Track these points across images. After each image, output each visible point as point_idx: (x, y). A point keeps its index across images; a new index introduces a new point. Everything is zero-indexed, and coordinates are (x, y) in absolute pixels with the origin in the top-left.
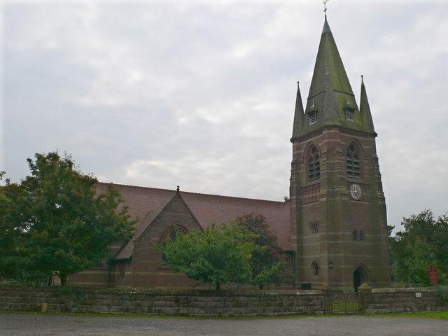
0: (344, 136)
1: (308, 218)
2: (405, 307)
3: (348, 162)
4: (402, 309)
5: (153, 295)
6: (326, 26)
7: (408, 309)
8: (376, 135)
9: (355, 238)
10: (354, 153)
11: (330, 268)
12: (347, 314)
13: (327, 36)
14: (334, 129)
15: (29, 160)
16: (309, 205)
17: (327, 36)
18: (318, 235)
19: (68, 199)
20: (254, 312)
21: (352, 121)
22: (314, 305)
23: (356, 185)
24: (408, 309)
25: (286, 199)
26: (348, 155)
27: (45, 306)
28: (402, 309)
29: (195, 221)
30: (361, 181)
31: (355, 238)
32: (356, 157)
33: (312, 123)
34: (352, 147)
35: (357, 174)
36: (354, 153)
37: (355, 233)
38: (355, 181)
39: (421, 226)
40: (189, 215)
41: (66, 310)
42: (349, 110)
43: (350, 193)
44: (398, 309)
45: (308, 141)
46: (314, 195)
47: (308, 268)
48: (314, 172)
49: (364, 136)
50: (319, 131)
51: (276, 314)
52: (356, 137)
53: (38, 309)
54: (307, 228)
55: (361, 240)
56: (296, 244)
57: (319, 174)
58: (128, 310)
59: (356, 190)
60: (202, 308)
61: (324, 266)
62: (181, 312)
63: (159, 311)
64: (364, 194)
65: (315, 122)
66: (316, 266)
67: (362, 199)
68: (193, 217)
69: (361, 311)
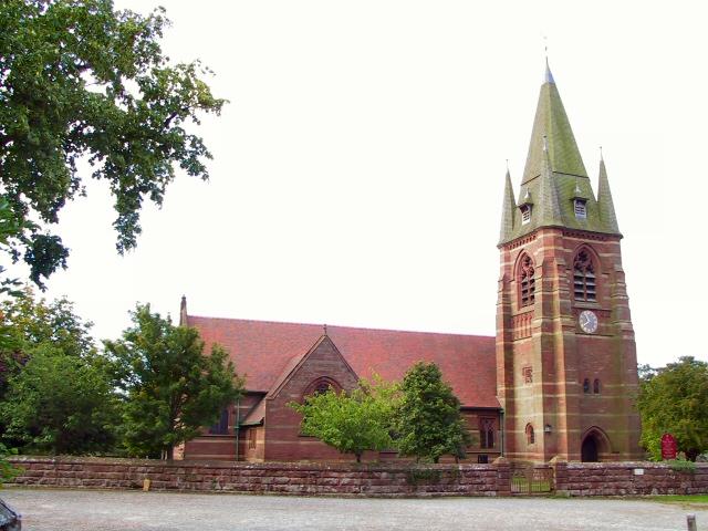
0: (570, 241)
1: (520, 362)
2: (618, 488)
3: (576, 278)
4: (612, 491)
5: (276, 470)
6: (550, 75)
7: (623, 492)
8: (620, 237)
9: (586, 390)
10: (587, 263)
11: (546, 433)
12: (531, 495)
13: (551, 94)
14: (572, 246)
15: (64, 267)
16: (522, 342)
17: (551, 94)
18: (531, 386)
19: (428, 414)
20: (400, 491)
21: (582, 220)
22: (482, 483)
23: (589, 312)
24: (623, 492)
25: (93, 74)
26: (577, 268)
27: (146, 483)
28: (612, 491)
29: (350, 370)
30: (597, 306)
31: (586, 390)
32: (589, 269)
33: (525, 222)
34: (582, 256)
35: (590, 296)
36: (587, 263)
37: (586, 383)
38: (588, 305)
39: (684, 377)
40: (340, 363)
41: (172, 489)
42: (578, 201)
43: (579, 325)
44: (607, 491)
45: (520, 248)
46: (528, 327)
47: (521, 431)
48: (526, 297)
49: (602, 239)
50: (531, 235)
51: (430, 494)
52: (587, 241)
53: (137, 487)
54: (519, 376)
55: (596, 391)
56: (504, 399)
57: (533, 297)
58: (243, 489)
59: (588, 322)
60: (334, 485)
61: (539, 431)
62: (309, 490)
63: (283, 490)
64: (602, 325)
65: (528, 221)
66: (530, 428)
67: (599, 332)
68: (346, 365)
69: (551, 493)
